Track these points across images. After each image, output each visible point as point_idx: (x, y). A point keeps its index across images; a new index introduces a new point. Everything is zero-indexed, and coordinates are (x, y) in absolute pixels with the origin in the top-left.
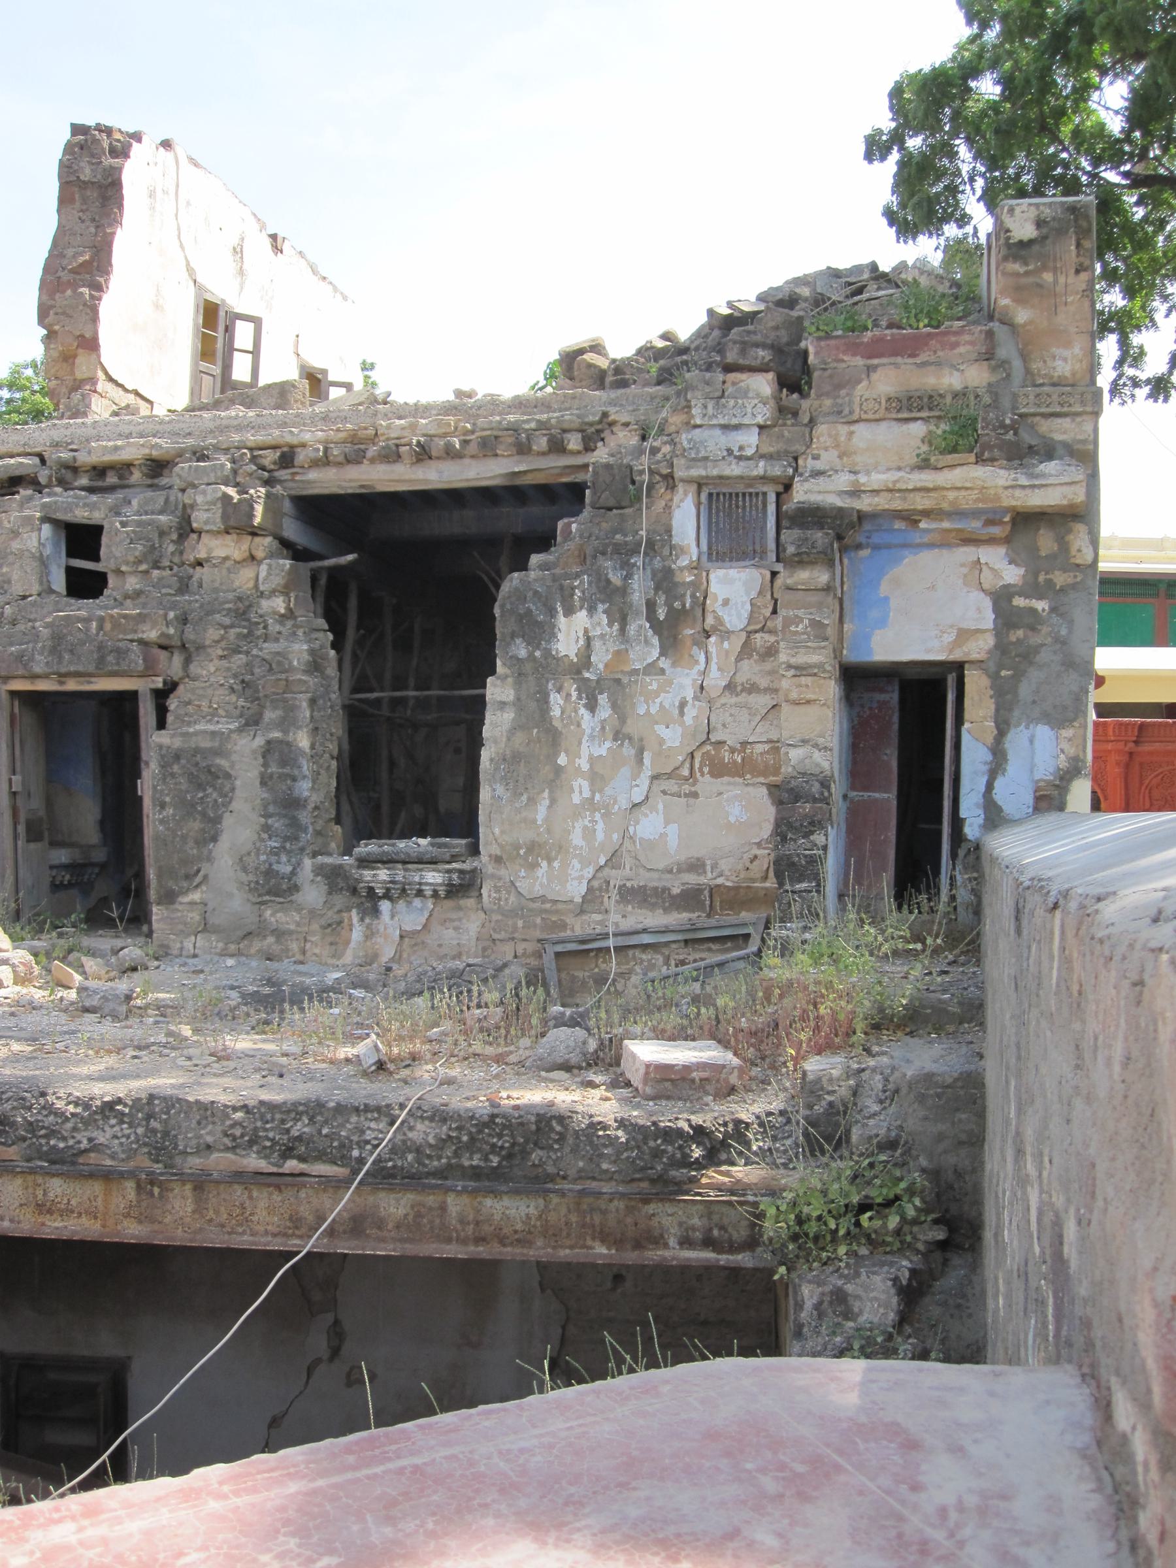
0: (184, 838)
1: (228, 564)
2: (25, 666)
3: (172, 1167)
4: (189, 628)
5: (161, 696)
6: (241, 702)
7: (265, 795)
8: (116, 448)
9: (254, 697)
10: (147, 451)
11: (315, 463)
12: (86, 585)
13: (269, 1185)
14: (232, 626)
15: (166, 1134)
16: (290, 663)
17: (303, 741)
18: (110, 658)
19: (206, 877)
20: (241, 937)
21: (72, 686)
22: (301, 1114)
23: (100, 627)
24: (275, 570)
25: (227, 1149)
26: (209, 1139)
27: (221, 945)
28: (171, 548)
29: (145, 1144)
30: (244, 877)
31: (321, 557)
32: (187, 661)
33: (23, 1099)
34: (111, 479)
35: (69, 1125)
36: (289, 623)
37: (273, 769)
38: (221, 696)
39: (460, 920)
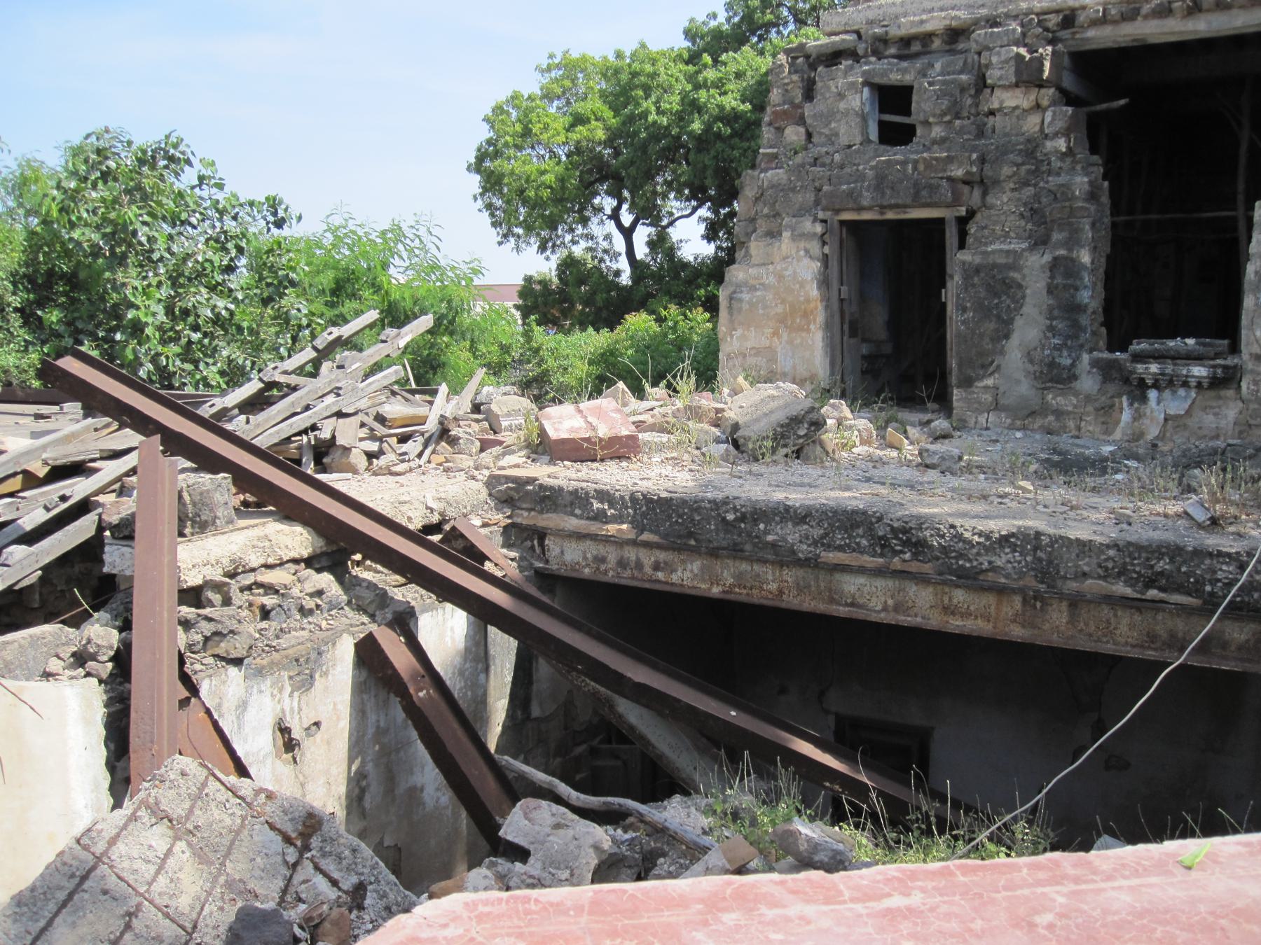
0: (981, 336)
1: (1017, 112)
2: (855, 201)
3: (1053, 587)
4: (987, 167)
5: (963, 222)
6: (1029, 226)
7: (1051, 302)
8: (922, 22)
9: (1041, 225)
10: (948, 22)
11: (1095, 23)
12: (896, 135)
13: (1131, 607)
14: (1023, 164)
15: (1050, 562)
16: (1073, 193)
17: (1085, 257)
18: (924, 193)
19: (999, 367)
20: (1024, 415)
21: (890, 215)
22: (1163, 554)
23: (915, 169)
24: (1056, 117)
25: (1100, 577)
26: (1086, 569)
27: (1009, 421)
28: (969, 101)
29: (1033, 569)
30: (1031, 368)
31: (1091, 104)
32: (984, 194)
33: (939, 529)
34: (916, 47)
35: (975, 551)
36: (1069, 160)
37: (1059, 280)
38: (1013, 222)
39: (1219, 407)
